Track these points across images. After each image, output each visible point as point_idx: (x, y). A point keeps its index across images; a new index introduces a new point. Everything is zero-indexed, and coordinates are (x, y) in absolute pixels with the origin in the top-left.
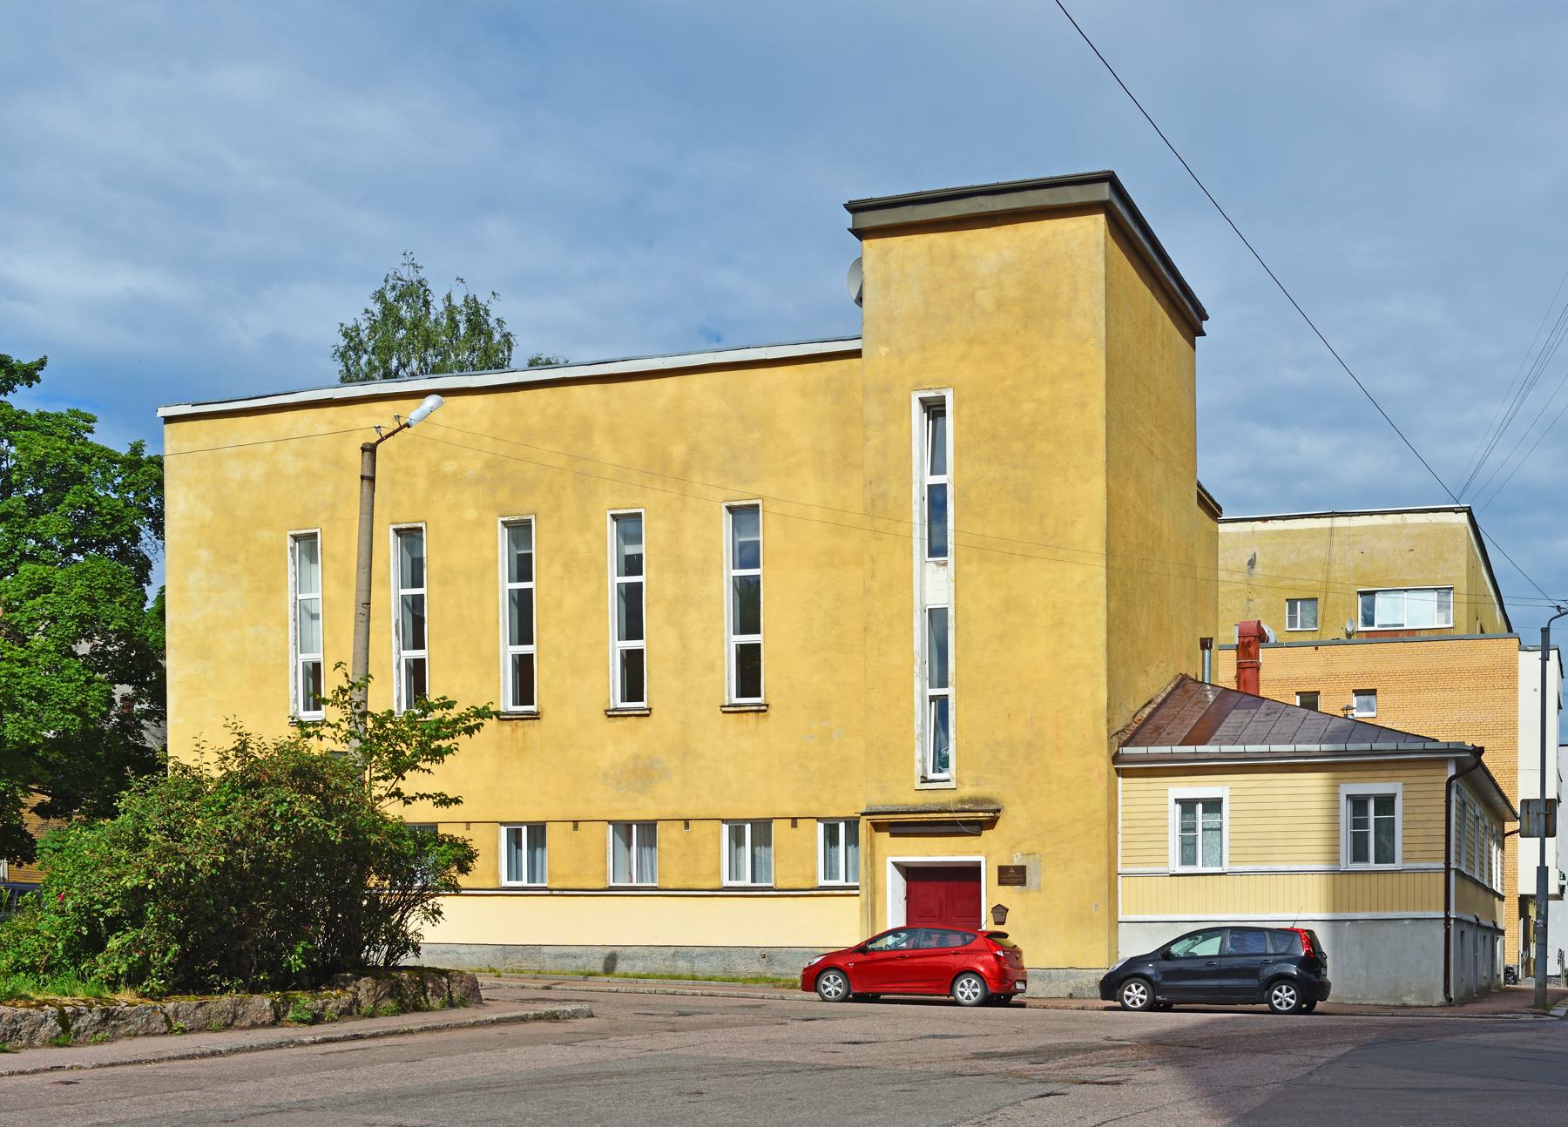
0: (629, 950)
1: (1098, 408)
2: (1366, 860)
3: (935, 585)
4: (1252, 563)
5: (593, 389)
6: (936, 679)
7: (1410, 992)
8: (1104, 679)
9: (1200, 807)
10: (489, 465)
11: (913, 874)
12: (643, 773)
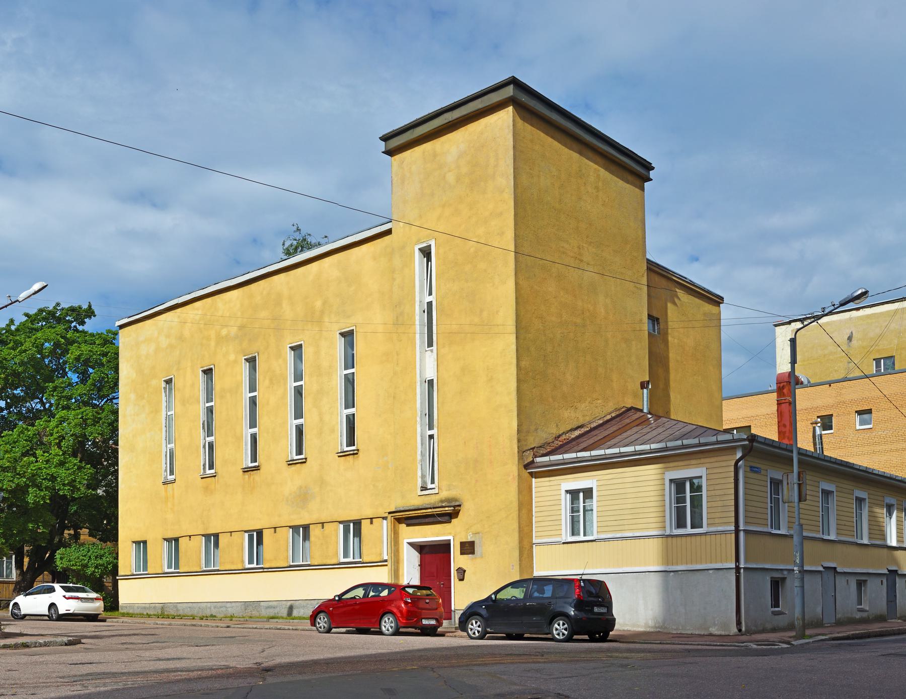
0: (297, 603)
1: (510, 234)
2: (685, 526)
3: (428, 365)
4: (850, 339)
5: (282, 276)
7: (715, 625)
8: (515, 413)
9: (581, 495)
10: (241, 327)
11: (421, 548)
12: (303, 497)
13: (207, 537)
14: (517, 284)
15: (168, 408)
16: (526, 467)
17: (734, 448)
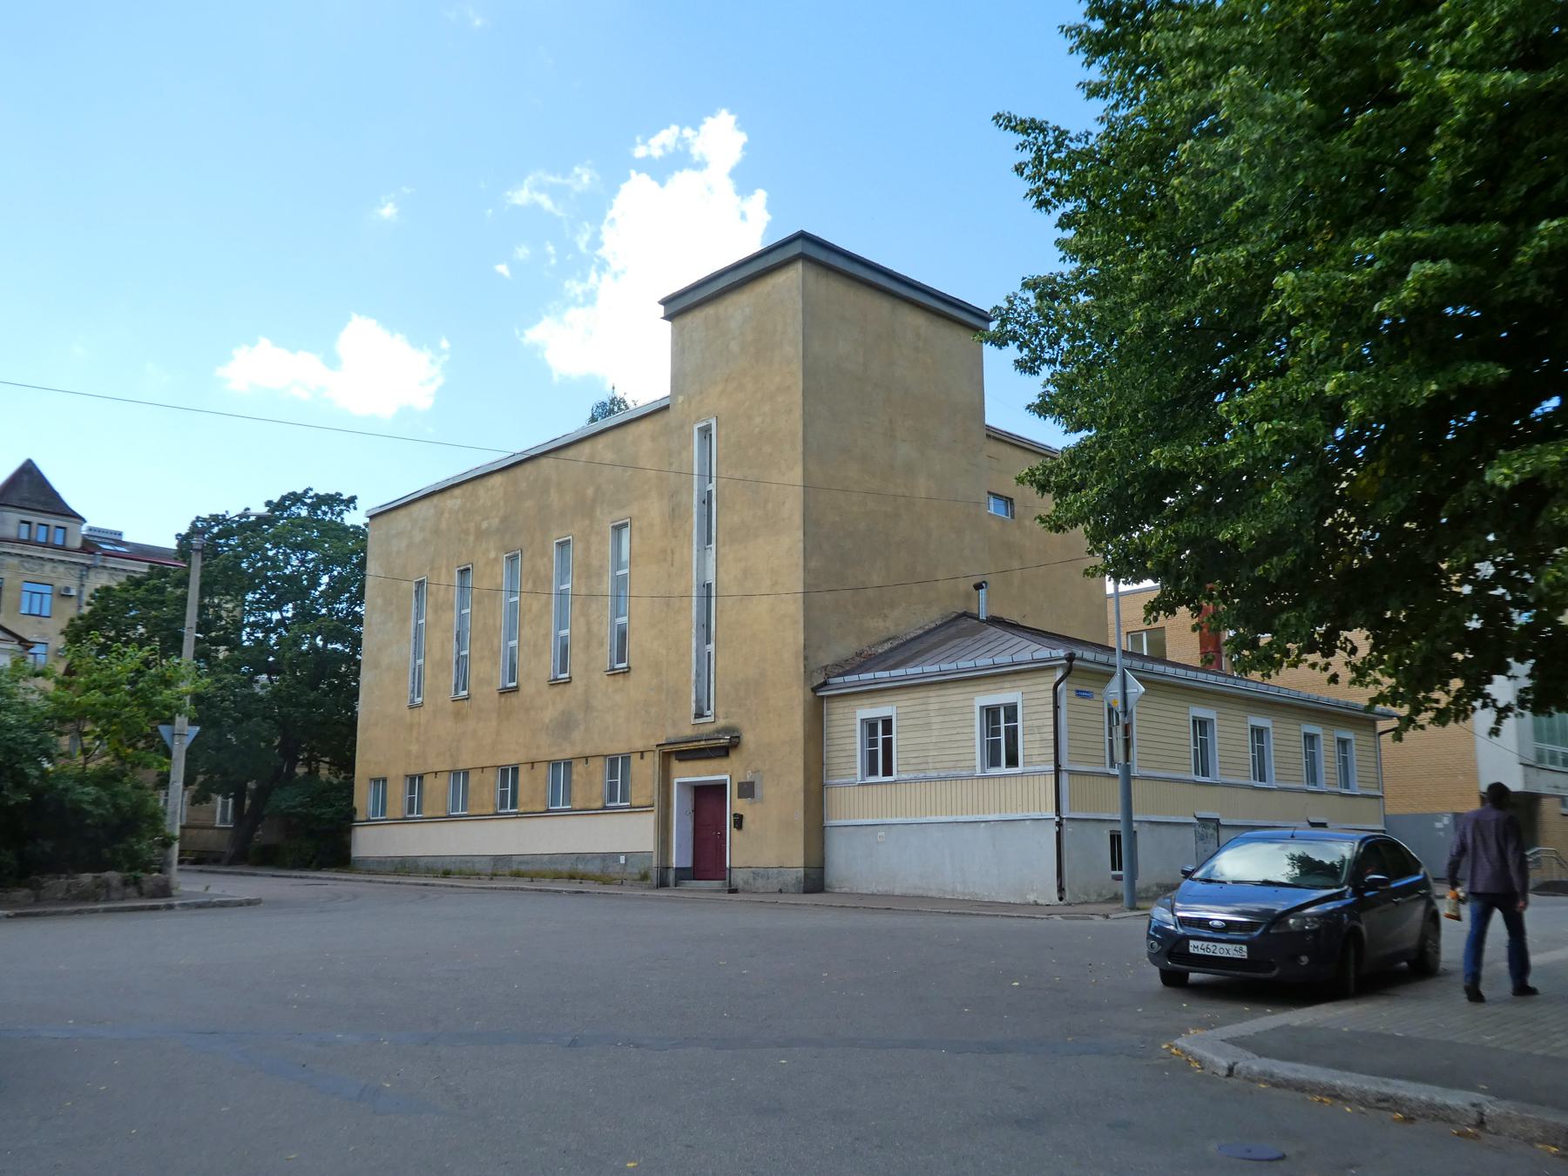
1: (798, 413)
5: (1173, 830)
6: (667, 749)
10: (504, 520)
12: (565, 725)
13: (456, 773)
14: (804, 469)
15: (419, 615)
16: (815, 690)
17: (1054, 668)
